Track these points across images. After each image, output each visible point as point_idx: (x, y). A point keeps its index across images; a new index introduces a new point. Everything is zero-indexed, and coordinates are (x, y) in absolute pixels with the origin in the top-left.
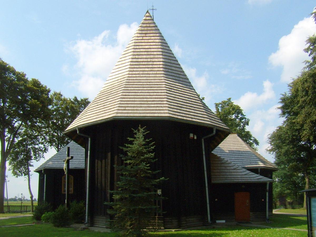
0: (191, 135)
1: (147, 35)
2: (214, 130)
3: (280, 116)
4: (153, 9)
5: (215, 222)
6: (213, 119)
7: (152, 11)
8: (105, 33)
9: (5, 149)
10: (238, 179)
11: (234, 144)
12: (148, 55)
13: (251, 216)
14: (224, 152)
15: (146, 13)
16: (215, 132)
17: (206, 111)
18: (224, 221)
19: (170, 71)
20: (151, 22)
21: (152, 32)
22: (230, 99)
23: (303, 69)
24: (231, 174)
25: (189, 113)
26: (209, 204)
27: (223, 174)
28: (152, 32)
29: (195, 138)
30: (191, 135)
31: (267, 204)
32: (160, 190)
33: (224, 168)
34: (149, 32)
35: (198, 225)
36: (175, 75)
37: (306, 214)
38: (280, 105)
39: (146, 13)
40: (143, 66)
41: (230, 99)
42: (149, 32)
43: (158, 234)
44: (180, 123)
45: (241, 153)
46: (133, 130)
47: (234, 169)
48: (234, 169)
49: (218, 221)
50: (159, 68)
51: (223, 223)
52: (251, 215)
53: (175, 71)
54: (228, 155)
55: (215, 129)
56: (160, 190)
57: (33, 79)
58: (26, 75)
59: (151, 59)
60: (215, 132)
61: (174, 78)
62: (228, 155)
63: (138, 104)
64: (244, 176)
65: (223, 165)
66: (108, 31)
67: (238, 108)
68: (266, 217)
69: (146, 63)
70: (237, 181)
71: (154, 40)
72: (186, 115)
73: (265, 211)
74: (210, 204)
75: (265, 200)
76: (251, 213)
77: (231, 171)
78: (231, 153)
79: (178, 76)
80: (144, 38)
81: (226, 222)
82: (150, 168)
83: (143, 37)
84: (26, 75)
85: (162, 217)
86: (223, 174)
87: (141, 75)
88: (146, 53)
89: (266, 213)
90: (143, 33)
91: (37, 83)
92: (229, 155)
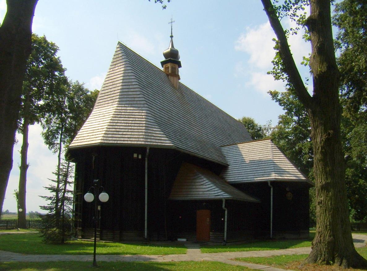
0: (135, 155)
1: (116, 66)
5: (177, 240)
10: (200, 195)
14: (244, 162)
16: (148, 151)
17: (155, 120)
18: (184, 240)
19: (125, 96)
21: (119, 62)
25: (238, 169)
27: (197, 193)
28: (119, 62)
30: (135, 155)
31: (226, 223)
32: (100, 206)
37: (96, 255)
38: (278, 122)
42: (118, 62)
43: (85, 252)
44: (158, 149)
45: (260, 163)
49: (179, 240)
52: (210, 235)
53: (113, 77)
56: (100, 206)
60: (148, 151)
61: (128, 102)
64: (208, 193)
68: (224, 239)
70: (203, 197)
73: (224, 232)
76: (211, 233)
80: (114, 69)
81: (187, 240)
86: (197, 193)
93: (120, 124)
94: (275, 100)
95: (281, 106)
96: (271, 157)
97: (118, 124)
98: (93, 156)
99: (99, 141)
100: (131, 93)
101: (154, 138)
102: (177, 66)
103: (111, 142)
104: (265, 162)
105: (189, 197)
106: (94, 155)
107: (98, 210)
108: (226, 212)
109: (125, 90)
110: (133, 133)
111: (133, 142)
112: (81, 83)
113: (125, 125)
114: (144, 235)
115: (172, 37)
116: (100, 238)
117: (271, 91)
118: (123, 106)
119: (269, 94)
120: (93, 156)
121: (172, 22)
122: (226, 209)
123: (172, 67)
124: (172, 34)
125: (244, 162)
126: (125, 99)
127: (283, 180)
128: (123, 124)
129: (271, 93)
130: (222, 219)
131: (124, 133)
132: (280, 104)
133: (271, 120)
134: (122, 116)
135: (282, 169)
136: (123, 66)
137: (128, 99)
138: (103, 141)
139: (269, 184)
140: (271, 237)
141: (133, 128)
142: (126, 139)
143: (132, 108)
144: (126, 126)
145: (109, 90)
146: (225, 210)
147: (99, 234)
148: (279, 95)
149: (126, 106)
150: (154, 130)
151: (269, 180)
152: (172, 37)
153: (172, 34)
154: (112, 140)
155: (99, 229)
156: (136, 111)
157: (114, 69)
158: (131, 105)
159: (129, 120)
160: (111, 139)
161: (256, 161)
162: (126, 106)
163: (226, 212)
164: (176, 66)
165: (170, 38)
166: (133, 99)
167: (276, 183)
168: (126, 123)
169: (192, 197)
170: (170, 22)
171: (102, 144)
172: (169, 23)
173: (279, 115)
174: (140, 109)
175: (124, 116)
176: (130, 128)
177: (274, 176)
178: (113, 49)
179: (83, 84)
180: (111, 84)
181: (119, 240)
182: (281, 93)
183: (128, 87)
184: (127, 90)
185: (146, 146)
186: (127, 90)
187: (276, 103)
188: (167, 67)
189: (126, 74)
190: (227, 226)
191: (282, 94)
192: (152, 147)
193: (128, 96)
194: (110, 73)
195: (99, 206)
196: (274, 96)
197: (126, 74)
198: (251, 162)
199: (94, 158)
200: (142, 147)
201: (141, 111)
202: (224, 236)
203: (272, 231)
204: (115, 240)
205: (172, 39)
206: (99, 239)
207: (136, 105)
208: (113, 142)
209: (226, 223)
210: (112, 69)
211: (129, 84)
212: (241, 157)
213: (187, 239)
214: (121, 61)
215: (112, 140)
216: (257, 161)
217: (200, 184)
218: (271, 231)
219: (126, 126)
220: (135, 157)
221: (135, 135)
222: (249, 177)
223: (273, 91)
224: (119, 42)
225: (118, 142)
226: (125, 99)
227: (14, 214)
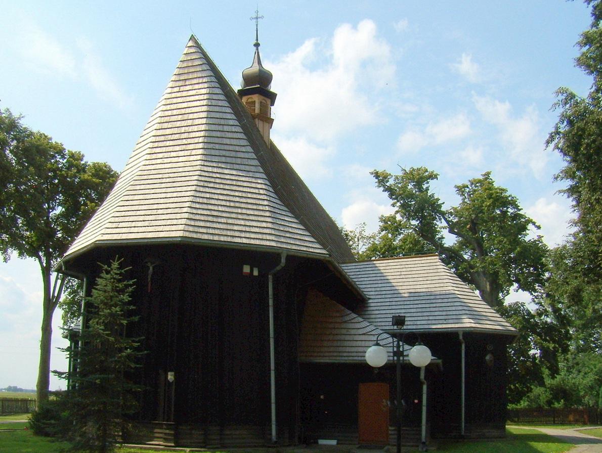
0: (246, 269)
1: (187, 83)
2: (282, 258)
3: (573, 209)
4: (257, 18)
5: (317, 443)
6: (288, 235)
7: (255, 20)
8: (307, 47)
9: (50, 294)
11: (425, 279)
12: (183, 120)
13: (391, 434)
14: (399, 295)
15: (189, 41)
16: (283, 260)
18: (334, 442)
19: (217, 147)
20: (195, 58)
21: (195, 75)
22: (488, 174)
23: (551, 108)
24: (354, 344)
26: (427, 407)
28: (195, 75)
29: (256, 273)
30: (246, 269)
31: (424, 409)
32: (173, 373)
33: (344, 331)
34: (191, 76)
35: (249, 444)
36: (227, 154)
39: (189, 41)
40: (171, 143)
41: (488, 174)
42: (191, 76)
45: (432, 297)
46: (101, 265)
47: (364, 334)
48: (364, 334)
49: (322, 442)
50: (197, 144)
51: (332, 446)
52: (390, 432)
54: (406, 303)
55: (285, 257)
56: (173, 373)
57: (94, 164)
58: (83, 156)
59: (187, 128)
60: (283, 260)
61: (223, 159)
62: (406, 303)
63: (141, 215)
65: (344, 326)
66: (313, 40)
67: (498, 194)
68: (420, 439)
69: (177, 137)
71: (198, 91)
72: (222, 231)
74: (277, 403)
75: (421, 402)
77: (356, 338)
78: (412, 299)
79: (233, 154)
80: (182, 89)
81: (338, 444)
82: (110, 332)
83: (181, 87)
84: (83, 156)
85: (172, 423)
87: (164, 161)
88: (180, 117)
89: (421, 431)
90: (180, 80)
91: (101, 170)
92: (408, 303)
93: (216, 201)
94: (382, 189)
95: (391, 200)
96: (450, 288)
97: (213, 202)
98: (149, 264)
99: (180, 234)
100: (228, 141)
101: (291, 236)
102: (269, 101)
103: (206, 237)
104: (442, 297)
105: (343, 358)
106: (152, 263)
107: (168, 381)
108: (425, 387)
109: (214, 134)
110: (248, 223)
111: (253, 242)
112: (15, 115)
113: (228, 204)
114: (271, 434)
115: (257, 45)
116: (174, 443)
117: (377, 170)
118: (215, 165)
119: (372, 176)
120: (149, 264)
121: (257, 18)
122: (425, 382)
123: (261, 102)
124: (257, 40)
125: (399, 295)
126: (217, 153)
127: (483, 329)
128: (223, 203)
129: (377, 175)
130: (416, 401)
131: (230, 221)
132: (391, 196)
133: (364, 223)
134: (217, 186)
135: (476, 311)
136: (206, 85)
137: (224, 153)
138: (187, 234)
139: (461, 337)
140: (463, 433)
141: (244, 211)
142: (237, 234)
143: (234, 172)
144: (230, 207)
145: (176, 130)
146: (422, 384)
147: (172, 432)
148: (389, 180)
149: (220, 165)
150: (286, 219)
151: (461, 329)
152: (257, 45)
153: (257, 40)
154: (207, 233)
155: (173, 423)
156: (243, 179)
157: (182, 89)
158: (232, 165)
159: (233, 196)
160: (204, 230)
161: (422, 294)
162: (220, 165)
163: (425, 387)
164: (267, 101)
165: (255, 48)
166: (233, 154)
167: (472, 336)
168: (230, 201)
169: (351, 358)
170: (254, 16)
171: (184, 239)
172: (252, 19)
173: (380, 216)
174: (251, 174)
175: (222, 186)
176: (239, 211)
177: (468, 323)
178: (182, 48)
179: (19, 118)
180: (180, 117)
181: (219, 446)
182: (394, 177)
183: (220, 128)
184: (218, 134)
185: (280, 251)
186: (218, 134)
187: (384, 192)
188: (250, 100)
189: (214, 103)
190: (465, 412)
191: (397, 178)
192: (292, 253)
193: (222, 147)
194: (174, 95)
195: (169, 373)
196: (382, 181)
197: (214, 103)
198: (412, 295)
199: (151, 268)
200: (264, 253)
201: (254, 180)
202: (420, 434)
203: (465, 423)
204: (211, 447)
205: (257, 49)
206: (173, 445)
207: (243, 167)
208: (211, 237)
209: (424, 409)
210: (178, 88)
211: (222, 122)
212: (388, 285)
213: (338, 440)
214: (199, 75)
215: (207, 233)
216: (425, 294)
217: (361, 332)
218: (463, 424)
219: (230, 207)
220: (245, 273)
221: (253, 226)
222: (419, 323)
223: (380, 170)
224: (192, 35)
225: (222, 239)
226: (217, 153)
227: (33, 391)
